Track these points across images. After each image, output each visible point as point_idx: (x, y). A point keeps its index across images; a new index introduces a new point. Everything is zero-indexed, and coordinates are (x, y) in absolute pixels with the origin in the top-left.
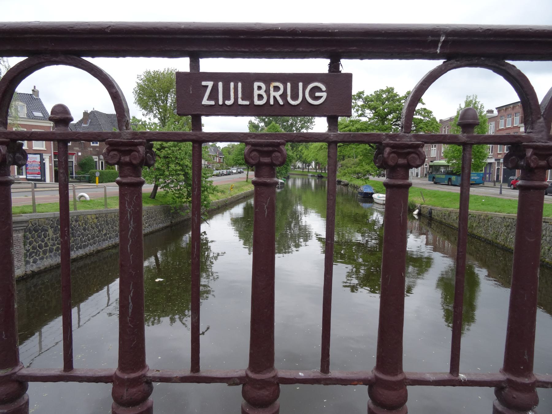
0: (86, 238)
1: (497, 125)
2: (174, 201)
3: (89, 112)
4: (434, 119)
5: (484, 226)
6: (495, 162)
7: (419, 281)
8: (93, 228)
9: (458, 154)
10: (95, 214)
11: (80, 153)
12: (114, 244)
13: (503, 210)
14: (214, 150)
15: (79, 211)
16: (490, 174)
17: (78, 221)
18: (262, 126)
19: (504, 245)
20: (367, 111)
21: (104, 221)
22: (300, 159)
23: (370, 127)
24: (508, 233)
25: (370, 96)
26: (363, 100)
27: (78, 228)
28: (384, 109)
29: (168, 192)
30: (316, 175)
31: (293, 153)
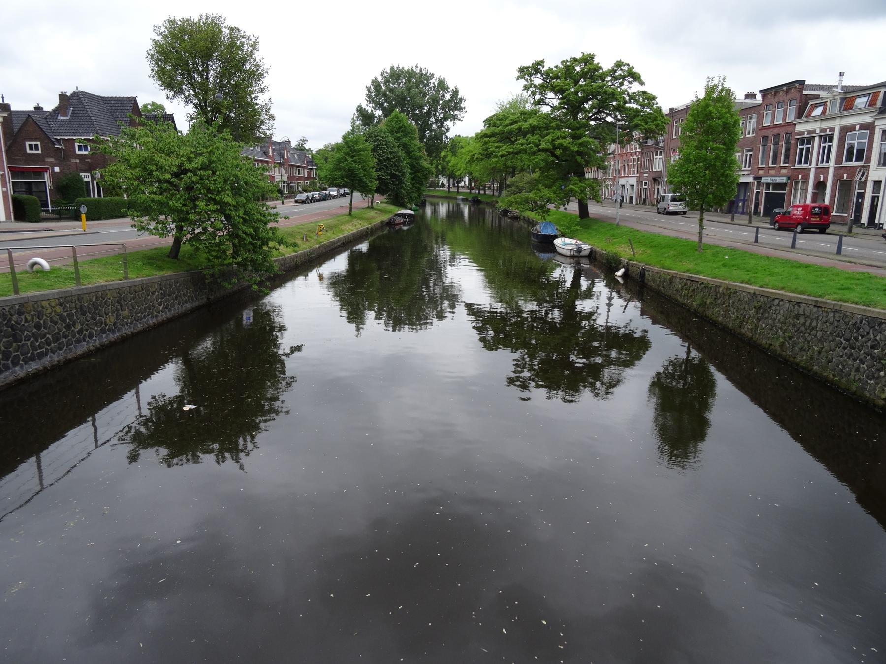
0: (43, 340)
1: (760, 120)
2: (209, 264)
3: (69, 94)
4: (659, 110)
5: (724, 304)
6: (753, 181)
7: (628, 372)
8: (56, 323)
9: (691, 179)
10: (58, 299)
11: (58, 168)
12: (99, 346)
13: (753, 281)
14: (299, 157)
15: (23, 294)
16: (744, 201)
17: (23, 314)
18: (379, 116)
19: (751, 338)
20: (550, 95)
21: (76, 308)
22: (443, 172)
23: (553, 124)
24: (759, 320)
25: (555, 69)
26: (542, 76)
27: (23, 325)
28: (576, 93)
29: (197, 249)
30: (470, 199)
31: (431, 163)
